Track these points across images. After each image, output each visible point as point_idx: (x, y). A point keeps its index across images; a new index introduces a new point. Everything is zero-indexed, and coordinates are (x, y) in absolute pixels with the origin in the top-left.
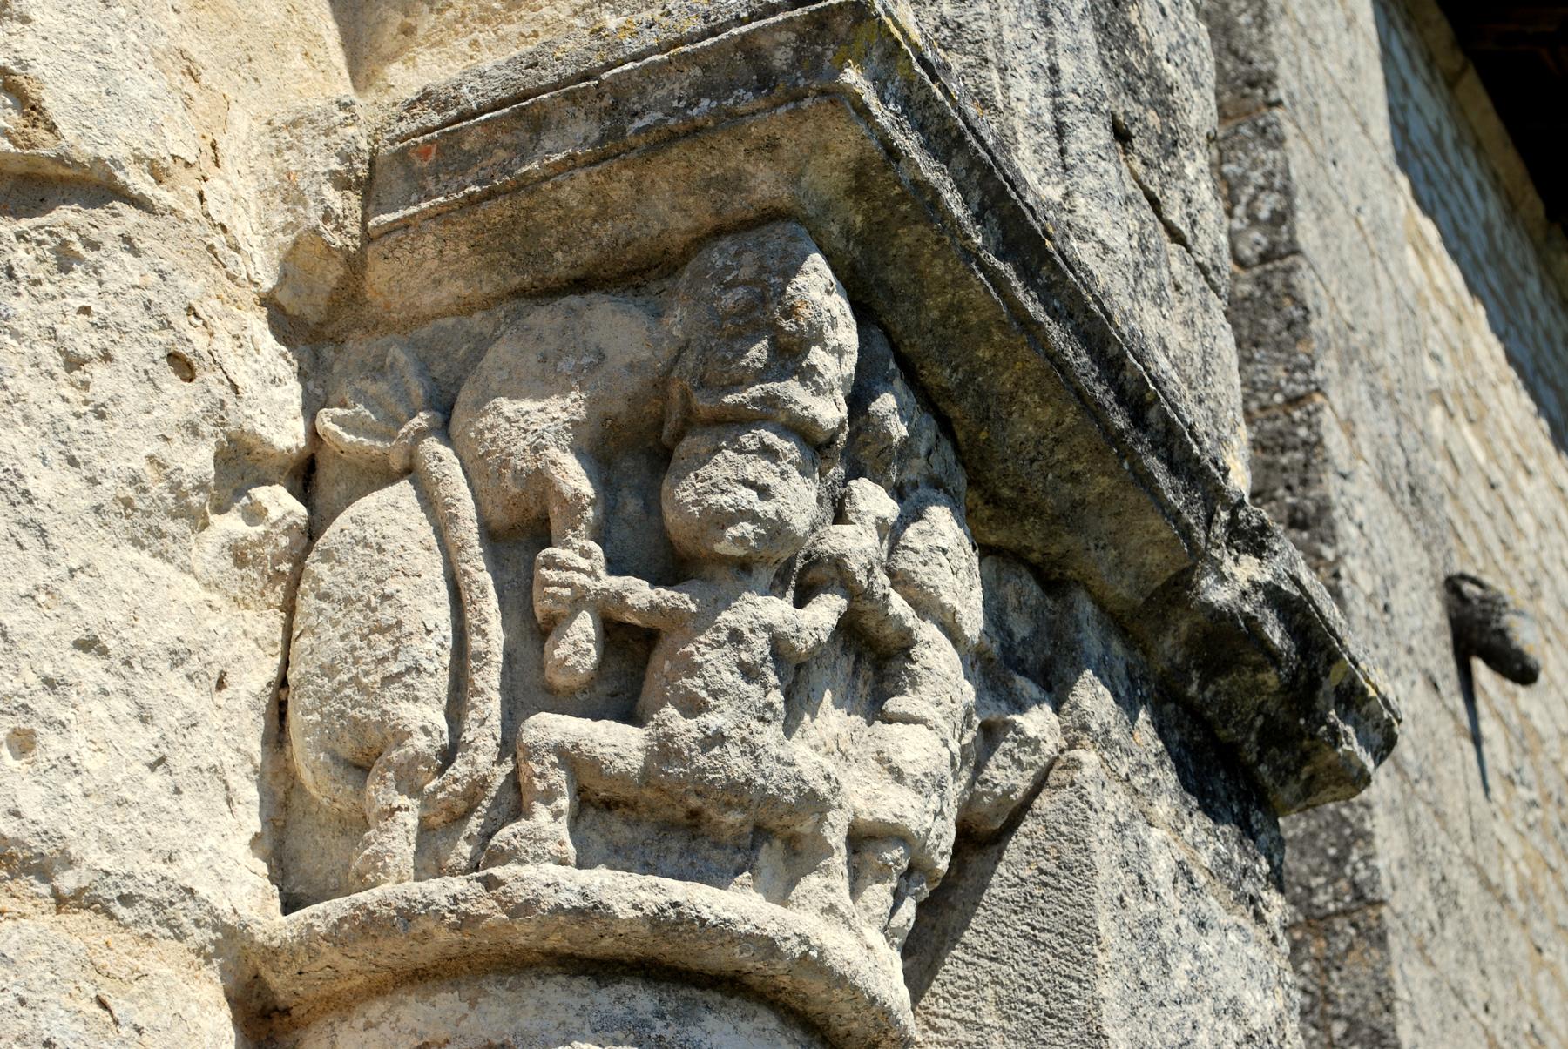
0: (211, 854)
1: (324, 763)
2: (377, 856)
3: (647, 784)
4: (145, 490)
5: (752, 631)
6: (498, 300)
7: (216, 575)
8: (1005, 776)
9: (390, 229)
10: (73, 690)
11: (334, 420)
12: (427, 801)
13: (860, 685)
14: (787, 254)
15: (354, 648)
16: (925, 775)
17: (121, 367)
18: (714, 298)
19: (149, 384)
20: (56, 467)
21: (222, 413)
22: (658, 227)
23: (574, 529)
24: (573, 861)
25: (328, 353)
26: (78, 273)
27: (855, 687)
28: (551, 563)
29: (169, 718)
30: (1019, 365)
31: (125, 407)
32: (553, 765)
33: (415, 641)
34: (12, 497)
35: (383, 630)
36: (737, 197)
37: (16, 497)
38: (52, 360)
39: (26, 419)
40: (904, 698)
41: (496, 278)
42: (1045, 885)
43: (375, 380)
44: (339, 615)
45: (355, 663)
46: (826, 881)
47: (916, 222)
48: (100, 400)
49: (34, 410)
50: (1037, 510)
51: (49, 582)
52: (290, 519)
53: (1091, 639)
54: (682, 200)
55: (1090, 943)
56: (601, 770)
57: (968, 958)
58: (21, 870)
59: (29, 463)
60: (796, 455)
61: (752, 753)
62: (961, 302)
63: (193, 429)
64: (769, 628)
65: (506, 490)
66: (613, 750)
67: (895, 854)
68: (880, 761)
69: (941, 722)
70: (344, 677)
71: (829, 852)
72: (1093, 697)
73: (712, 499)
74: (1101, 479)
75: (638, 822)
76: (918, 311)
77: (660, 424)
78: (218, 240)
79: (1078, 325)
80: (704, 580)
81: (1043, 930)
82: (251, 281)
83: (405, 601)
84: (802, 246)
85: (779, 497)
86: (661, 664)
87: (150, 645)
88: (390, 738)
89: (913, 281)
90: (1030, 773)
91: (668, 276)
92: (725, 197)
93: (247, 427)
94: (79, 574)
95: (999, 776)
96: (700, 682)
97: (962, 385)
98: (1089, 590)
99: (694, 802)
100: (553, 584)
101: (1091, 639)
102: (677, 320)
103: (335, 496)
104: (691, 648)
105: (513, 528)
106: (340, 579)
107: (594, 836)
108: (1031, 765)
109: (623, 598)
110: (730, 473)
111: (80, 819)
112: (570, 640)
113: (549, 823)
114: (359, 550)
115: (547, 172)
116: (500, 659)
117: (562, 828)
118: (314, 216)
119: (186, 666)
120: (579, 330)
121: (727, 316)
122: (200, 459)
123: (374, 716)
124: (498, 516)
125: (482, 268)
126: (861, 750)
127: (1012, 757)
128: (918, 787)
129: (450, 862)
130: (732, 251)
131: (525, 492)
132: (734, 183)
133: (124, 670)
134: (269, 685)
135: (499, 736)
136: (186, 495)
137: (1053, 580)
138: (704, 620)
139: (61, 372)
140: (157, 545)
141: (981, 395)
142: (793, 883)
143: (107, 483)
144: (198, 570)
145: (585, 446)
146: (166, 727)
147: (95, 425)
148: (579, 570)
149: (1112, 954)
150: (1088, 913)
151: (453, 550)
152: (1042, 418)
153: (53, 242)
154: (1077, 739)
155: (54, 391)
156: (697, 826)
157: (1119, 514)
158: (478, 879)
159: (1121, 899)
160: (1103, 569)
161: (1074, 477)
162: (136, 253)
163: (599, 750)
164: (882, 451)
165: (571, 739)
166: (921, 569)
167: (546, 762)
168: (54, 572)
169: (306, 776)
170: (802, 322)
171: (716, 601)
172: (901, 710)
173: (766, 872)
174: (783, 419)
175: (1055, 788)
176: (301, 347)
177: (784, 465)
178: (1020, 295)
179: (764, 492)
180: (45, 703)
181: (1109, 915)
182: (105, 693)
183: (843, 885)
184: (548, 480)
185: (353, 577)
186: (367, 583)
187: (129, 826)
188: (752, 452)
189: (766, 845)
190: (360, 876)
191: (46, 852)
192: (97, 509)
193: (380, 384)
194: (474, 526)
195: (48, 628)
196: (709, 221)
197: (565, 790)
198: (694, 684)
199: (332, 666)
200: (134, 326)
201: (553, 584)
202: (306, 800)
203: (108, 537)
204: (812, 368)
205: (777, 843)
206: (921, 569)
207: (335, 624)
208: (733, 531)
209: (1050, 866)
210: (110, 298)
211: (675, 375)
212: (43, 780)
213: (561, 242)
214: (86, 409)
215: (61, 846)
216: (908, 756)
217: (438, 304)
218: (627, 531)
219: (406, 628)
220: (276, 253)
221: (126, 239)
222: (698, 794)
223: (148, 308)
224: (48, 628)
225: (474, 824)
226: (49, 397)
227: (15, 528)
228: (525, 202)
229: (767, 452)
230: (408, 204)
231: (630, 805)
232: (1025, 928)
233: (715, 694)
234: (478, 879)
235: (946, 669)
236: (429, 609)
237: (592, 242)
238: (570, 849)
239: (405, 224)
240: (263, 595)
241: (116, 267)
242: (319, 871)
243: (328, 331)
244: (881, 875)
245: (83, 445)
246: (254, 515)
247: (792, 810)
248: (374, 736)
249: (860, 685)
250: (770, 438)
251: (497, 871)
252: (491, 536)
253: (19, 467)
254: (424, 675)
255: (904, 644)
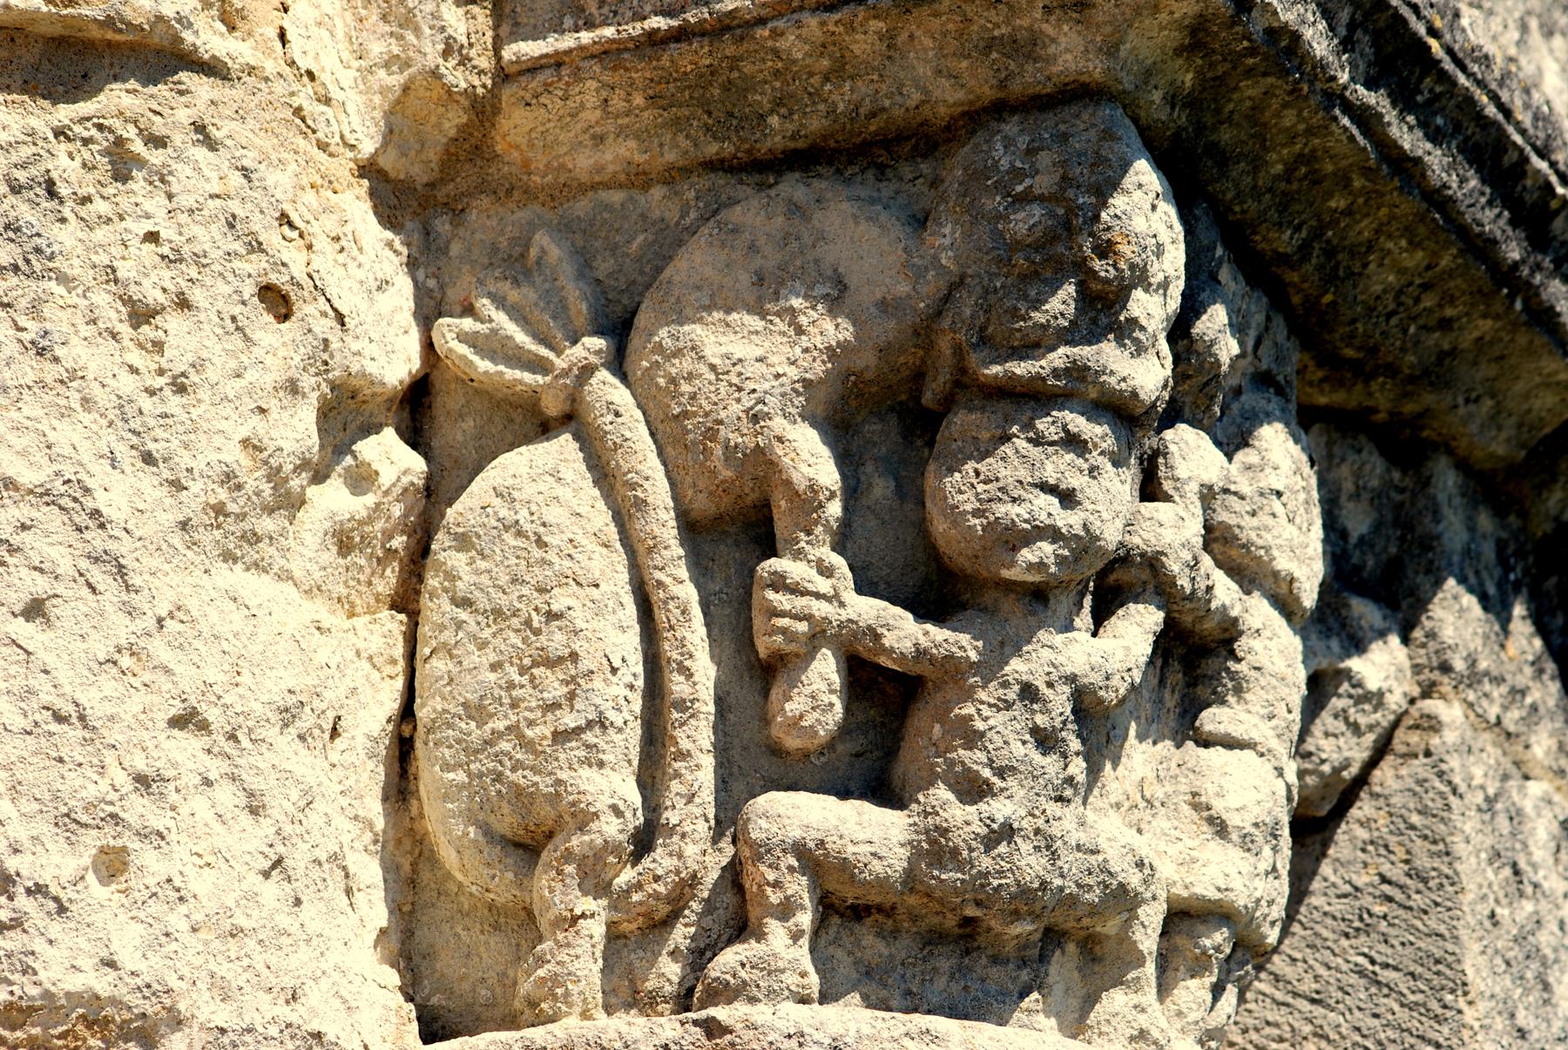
0: (336, 976)
1: (475, 841)
2: (555, 979)
3: (912, 890)
4: (239, 487)
5: (1050, 685)
6: (686, 171)
7: (317, 575)
8: (1340, 749)
9: (534, 67)
10: (171, 786)
11: (463, 337)
12: (618, 901)
13: (1167, 695)
14: (1099, 161)
15: (511, 686)
16: (1256, 825)
17: (202, 316)
18: (1000, 217)
19: (238, 336)
20: (128, 469)
21: (325, 356)
22: (916, 97)
23: (809, 533)
24: (816, 996)
25: (442, 225)
26: (138, 183)
27: (1161, 701)
28: (779, 583)
29: (280, 805)
30: (1384, 211)
31: (212, 374)
32: (791, 869)
33: (597, 683)
34: (77, 520)
35: (552, 663)
36: (1029, 68)
37: (82, 519)
38: (113, 314)
39: (86, 402)
40: (1225, 710)
41: (684, 143)
42: (1390, 899)
43: (516, 283)
44: (487, 633)
45: (514, 705)
46: (1136, 999)
47: (1265, 74)
48: (179, 368)
49: (96, 391)
50: (1392, 370)
51: (133, 639)
52: (405, 480)
53: (1456, 523)
54: (951, 63)
55: (1453, 991)
56: (853, 875)
57: (1279, 996)
58: (119, 1037)
59: (94, 467)
60: (1109, 443)
61: (1048, 847)
62: (1314, 150)
63: (293, 388)
64: (1071, 679)
65: (713, 472)
66: (868, 848)
67: (1217, 939)
68: (1196, 807)
69: (1274, 743)
70: (500, 725)
71: (1140, 961)
72: (1456, 615)
73: (1001, 510)
74: (1481, 322)
75: (896, 933)
76: (1256, 170)
77: (919, 377)
78: (304, 99)
79: (1467, 139)
80: (984, 610)
81: (1386, 966)
82: (346, 144)
83: (580, 624)
84: (1120, 148)
85: (1087, 504)
86: (924, 727)
87: (257, 707)
88: (567, 818)
89: (1253, 136)
90: (1370, 738)
91: (924, 156)
92: (1013, 66)
93: (354, 369)
94: (168, 622)
95: (1327, 745)
96: (981, 756)
97: (1305, 247)
98: (1450, 452)
99: (971, 911)
100: (783, 614)
101: (1453, 530)
102: (947, 240)
103: (460, 437)
104: (969, 709)
105: (719, 518)
106: (485, 579)
107: (839, 953)
108: (1371, 728)
109: (877, 637)
110: (1023, 473)
111: (189, 963)
112: (807, 690)
113: (784, 946)
114: (509, 538)
115: (763, 12)
116: (711, 708)
117: (802, 954)
118: (432, 53)
119: (298, 724)
120: (807, 239)
121: (1016, 246)
122: (301, 427)
123: (545, 785)
124: (702, 504)
125: (663, 126)
126: (1169, 788)
127: (1346, 720)
128: (1247, 843)
129: (650, 985)
130: (1023, 142)
131: (740, 476)
132: (1027, 47)
133: (229, 747)
134: (389, 721)
135: (711, 816)
136: (286, 480)
137: (1407, 445)
138: (990, 667)
139: (125, 330)
140: (252, 555)
141: (1330, 252)
142: (1091, 1000)
143: (196, 487)
144: (297, 574)
145: (820, 411)
146: (282, 818)
147: (174, 403)
148: (818, 596)
149: (1483, 1006)
150: (1450, 947)
151: (641, 550)
152: (1410, 264)
153: (103, 141)
154: (1433, 684)
155: (118, 359)
156: (971, 937)
157: (1502, 357)
158: (696, 1023)
159: (1493, 915)
160: (1473, 428)
161: (1445, 325)
162: (211, 144)
163: (851, 849)
164: (1207, 384)
165: (814, 834)
166: (1248, 522)
167: (783, 866)
168: (140, 624)
169: (448, 855)
170: (1123, 265)
171: (1002, 644)
172: (1222, 729)
173: (1058, 990)
174: (1093, 395)
175: (1403, 756)
176: (409, 225)
177: (1095, 458)
178: (1394, 131)
179: (1068, 498)
180: (138, 809)
181: (1477, 947)
182: (208, 783)
183: (1150, 995)
184: (772, 463)
185: (504, 579)
186: (525, 591)
187: (246, 962)
188: (1052, 444)
189: (1058, 953)
190: (533, 1004)
191: (150, 1011)
192: (184, 525)
193: (525, 290)
194: (669, 517)
195: (135, 704)
196: (988, 93)
197: (807, 902)
198: (974, 758)
199: (480, 707)
200: (215, 254)
201: (783, 614)
202: (439, 874)
203: (197, 560)
204: (1133, 322)
205: (1071, 947)
206: (1248, 522)
207: (482, 645)
208: (1027, 555)
209: (1397, 873)
210: (183, 218)
211: (946, 323)
212: (142, 915)
213: (778, 103)
214: (160, 382)
215: (168, 1002)
216: (1233, 801)
217: (600, 169)
218: (873, 523)
219: (586, 664)
220: (377, 99)
221: (200, 128)
222: (978, 903)
223: (231, 226)
224: (135, 704)
225: (681, 935)
226: (106, 363)
227: (84, 564)
228: (730, 50)
229: (1073, 442)
230: (560, 30)
231: (888, 911)
232: (1361, 960)
233: (1001, 773)
234: (696, 1023)
235: (1279, 665)
236: (613, 636)
237: (822, 107)
238: (814, 979)
239: (557, 61)
240: (370, 583)
241: (189, 172)
242: (462, 978)
243: (441, 194)
244: (1198, 967)
245: (159, 433)
246: (361, 480)
247: (1094, 911)
248: (545, 812)
249: (1167, 695)
250: (1078, 423)
251: (720, 1013)
252: (691, 528)
253: (83, 476)
254: (611, 731)
255: (1227, 635)
